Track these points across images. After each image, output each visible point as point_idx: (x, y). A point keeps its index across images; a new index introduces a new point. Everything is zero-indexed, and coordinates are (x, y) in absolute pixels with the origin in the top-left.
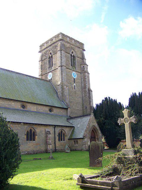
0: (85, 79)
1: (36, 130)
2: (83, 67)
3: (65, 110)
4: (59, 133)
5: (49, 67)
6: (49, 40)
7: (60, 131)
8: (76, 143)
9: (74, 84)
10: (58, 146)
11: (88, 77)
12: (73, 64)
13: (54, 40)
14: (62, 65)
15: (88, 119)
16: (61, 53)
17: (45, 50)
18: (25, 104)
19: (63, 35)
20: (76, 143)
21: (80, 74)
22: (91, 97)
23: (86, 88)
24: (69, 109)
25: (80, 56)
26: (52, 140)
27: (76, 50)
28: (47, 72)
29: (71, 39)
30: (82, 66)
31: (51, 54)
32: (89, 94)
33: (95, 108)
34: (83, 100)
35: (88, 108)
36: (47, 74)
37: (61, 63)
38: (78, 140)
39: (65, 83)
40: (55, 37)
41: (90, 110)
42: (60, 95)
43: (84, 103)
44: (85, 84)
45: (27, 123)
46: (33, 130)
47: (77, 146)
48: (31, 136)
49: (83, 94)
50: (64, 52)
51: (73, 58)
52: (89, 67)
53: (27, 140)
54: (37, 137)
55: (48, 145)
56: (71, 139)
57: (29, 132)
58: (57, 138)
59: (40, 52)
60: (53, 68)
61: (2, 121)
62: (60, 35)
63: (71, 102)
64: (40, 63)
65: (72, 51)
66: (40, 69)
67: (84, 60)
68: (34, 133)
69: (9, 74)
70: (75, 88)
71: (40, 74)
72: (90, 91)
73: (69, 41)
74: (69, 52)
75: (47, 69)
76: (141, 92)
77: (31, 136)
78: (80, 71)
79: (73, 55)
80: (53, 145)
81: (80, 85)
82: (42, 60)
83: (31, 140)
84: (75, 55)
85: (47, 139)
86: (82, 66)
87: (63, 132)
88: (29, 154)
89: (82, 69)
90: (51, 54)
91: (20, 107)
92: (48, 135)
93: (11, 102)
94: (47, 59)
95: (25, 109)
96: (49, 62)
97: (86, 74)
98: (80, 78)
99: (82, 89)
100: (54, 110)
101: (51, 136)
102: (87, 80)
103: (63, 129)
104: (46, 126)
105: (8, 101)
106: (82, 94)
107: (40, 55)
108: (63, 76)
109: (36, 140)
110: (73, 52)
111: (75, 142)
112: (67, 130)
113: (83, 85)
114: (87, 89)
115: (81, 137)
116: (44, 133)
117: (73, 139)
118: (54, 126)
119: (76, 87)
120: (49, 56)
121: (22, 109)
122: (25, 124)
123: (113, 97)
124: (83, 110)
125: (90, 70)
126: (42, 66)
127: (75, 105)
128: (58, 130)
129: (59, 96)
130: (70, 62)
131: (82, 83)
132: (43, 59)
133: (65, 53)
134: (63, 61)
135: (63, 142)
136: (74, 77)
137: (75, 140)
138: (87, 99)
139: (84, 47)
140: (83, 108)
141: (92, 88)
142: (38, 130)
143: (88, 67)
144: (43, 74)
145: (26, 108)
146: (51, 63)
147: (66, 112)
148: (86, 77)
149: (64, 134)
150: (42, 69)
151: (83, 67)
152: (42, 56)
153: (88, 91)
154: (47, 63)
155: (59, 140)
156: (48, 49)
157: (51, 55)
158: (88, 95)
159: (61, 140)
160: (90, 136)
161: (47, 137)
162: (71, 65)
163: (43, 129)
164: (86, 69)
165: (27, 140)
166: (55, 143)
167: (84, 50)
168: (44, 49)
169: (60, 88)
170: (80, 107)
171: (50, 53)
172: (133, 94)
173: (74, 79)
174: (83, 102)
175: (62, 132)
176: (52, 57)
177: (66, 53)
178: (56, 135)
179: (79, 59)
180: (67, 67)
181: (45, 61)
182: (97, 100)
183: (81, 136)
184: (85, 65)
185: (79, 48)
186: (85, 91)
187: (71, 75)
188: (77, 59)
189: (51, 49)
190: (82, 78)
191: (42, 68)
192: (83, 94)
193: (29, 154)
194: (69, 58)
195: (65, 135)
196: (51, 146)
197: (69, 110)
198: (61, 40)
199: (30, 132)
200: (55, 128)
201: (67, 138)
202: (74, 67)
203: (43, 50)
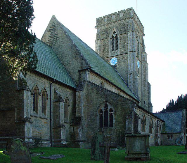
2: (144, 56)
8: (170, 138)
20: (170, 138)
25: (142, 43)
28: (109, 56)
34: (142, 94)
38: (174, 135)
47: (171, 141)
52: (148, 57)
69: (88, 48)
72: (149, 85)
76: (184, 95)
90: (114, 33)
107: (96, 30)
113: (143, 77)
114: (146, 83)
115: (178, 131)
138: (147, 94)
143: (147, 55)
151: (144, 56)
154: (109, 44)
157: (114, 35)
158: (147, 89)
171: (113, 32)
186: (145, 85)
190: (143, 69)
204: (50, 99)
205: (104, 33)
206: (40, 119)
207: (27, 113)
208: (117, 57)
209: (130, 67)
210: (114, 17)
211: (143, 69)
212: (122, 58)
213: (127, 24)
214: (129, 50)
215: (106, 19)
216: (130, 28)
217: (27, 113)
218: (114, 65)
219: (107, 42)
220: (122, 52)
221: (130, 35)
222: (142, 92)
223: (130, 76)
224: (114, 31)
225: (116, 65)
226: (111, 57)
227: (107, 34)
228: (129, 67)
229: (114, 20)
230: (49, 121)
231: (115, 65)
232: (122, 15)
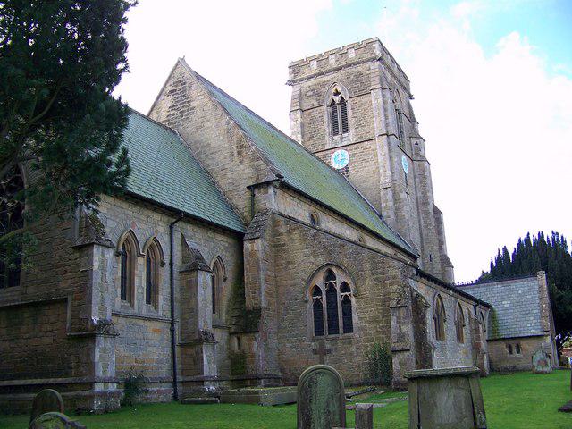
2: (416, 143)
6: (329, 53)
8: (514, 350)
13: (352, 55)
16: (384, 96)
17: (315, 81)
20: (514, 350)
30: (414, 141)
31: (337, 93)
38: (524, 344)
40: (357, 47)
47: (519, 359)
56: (496, 340)
59: (291, 83)
75: (327, 138)
111: (510, 348)
113: (419, 194)
115: (533, 332)
117: (504, 339)
126: (302, 125)
129: (389, 222)
137: (510, 342)
141: (440, 199)
151: (416, 143)
152: (301, 97)
153: (432, 213)
154: (326, 118)
156: (326, 78)
157: (337, 99)
158: (433, 224)
167: (411, 97)
171: (334, 91)
181: (316, 113)
186: (426, 213)
204: (171, 264)
206: (141, 322)
207: (102, 309)
208: (348, 148)
210: (332, 59)
217: (102, 309)
219: (320, 115)
228: (381, 171)
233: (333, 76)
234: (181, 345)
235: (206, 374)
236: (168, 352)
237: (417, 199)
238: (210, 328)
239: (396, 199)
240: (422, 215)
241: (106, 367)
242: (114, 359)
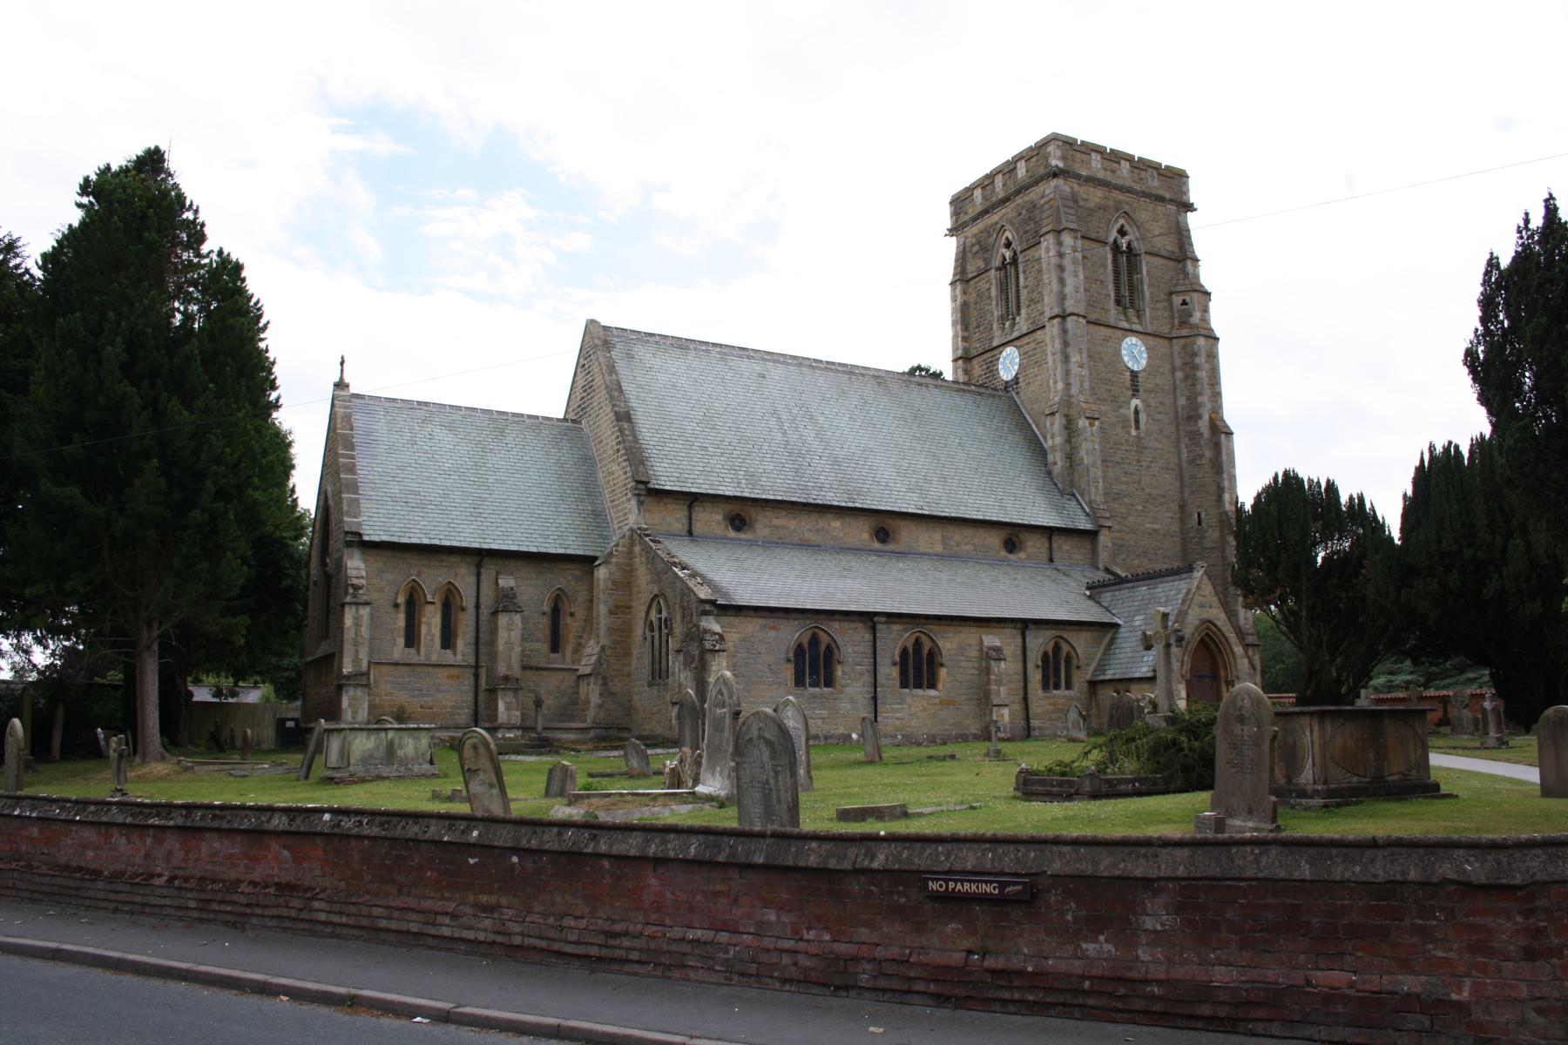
0: (1195, 367)
1: (940, 643)
2: (1184, 303)
3: (1086, 546)
4: (1045, 654)
5: (1003, 319)
7: (1051, 645)
9: (1135, 402)
10: (1039, 710)
11: (1213, 356)
12: (1128, 296)
14: (1069, 311)
15: (1179, 590)
16: (1060, 243)
18: (888, 521)
19: (1068, 144)
21: (1165, 343)
22: (1225, 466)
23: (1200, 417)
24: (1104, 532)
26: (1013, 686)
27: (1143, 216)
28: (995, 344)
29: (1115, 157)
30: (1177, 300)
31: (1008, 245)
32: (1217, 447)
33: (1466, 454)
34: (1182, 482)
35: (1210, 518)
36: (996, 352)
37: (1062, 297)
39: (1080, 399)
41: (1221, 531)
42: (1059, 464)
43: (1186, 495)
44: (1196, 397)
45: (900, 616)
46: (824, 639)
48: (918, 668)
49: (1184, 450)
50: (1076, 238)
51: (1127, 260)
52: (1213, 306)
53: (904, 685)
54: (943, 672)
55: (995, 709)
57: (1051, 655)
58: (1035, 676)
60: (1023, 325)
61: (173, 239)
62: (1051, 148)
63: (1118, 497)
64: (958, 291)
65: (1122, 221)
66: (959, 327)
67: (1189, 263)
68: (931, 653)
70: (1137, 422)
71: (960, 353)
72: (1220, 432)
73: (1100, 175)
74: (1102, 236)
75: (995, 326)
77: (918, 668)
78: (1165, 330)
79: (1124, 242)
80: (1018, 707)
81: (1168, 400)
82: (962, 278)
83: (918, 686)
84: (1135, 244)
85: (988, 683)
86: (1177, 300)
87: (1065, 648)
88: (911, 741)
89: (1176, 314)
91: (866, 536)
92: (992, 662)
93: (829, 516)
94: (993, 273)
95: (891, 547)
96: (1003, 288)
97: (1201, 341)
98: (1168, 367)
99: (1178, 426)
100: (1029, 543)
101: (1007, 668)
102: (1203, 374)
103: (1065, 635)
104: (984, 624)
105: (814, 516)
106: (1179, 453)
107: (952, 245)
108: (1074, 369)
109: (940, 686)
110: (1127, 228)
112: (1081, 643)
113: (1182, 401)
114: (1203, 426)
116: (974, 653)
117: (1111, 681)
118: (1019, 626)
119: (1143, 417)
120: (999, 258)
121: (877, 545)
122: (891, 620)
123: (1312, 471)
124: (1184, 534)
125: (1220, 318)
127: (1140, 508)
128: (1039, 643)
130: (1111, 287)
131: (1175, 389)
132: (972, 269)
133: (1079, 243)
134: (1068, 290)
135: (1067, 693)
136: (1130, 365)
137: (432, 579)
139: (1186, 193)
140: (1182, 521)
142: (948, 643)
144: (974, 353)
145: (894, 539)
146: (1012, 296)
147: (1089, 547)
148: (1201, 360)
149: (1068, 659)
150: (965, 327)
151: (1184, 303)
154: (994, 292)
155: (1045, 687)
157: (1008, 254)
158: (1208, 454)
159: (1057, 687)
160: (1187, 667)
161: (988, 674)
162: (1118, 302)
163: (969, 636)
164: (1197, 315)
165: (904, 685)
166: (1025, 699)
167: (1189, 207)
168: (975, 219)
169: (1056, 428)
170: (1165, 520)
171: (1003, 241)
172: (1432, 448)
173: (1134, 375)
174: (1182, 492)
175: (1057, 648)
176: (1014, 260)
177: (1087, 243)
178: (1030, 665)
179: (1162, 261)
180: (1093, 317)
181: (983, 285)
182: (1248, 487)
183: (1145, 669)
184: (1195, 295)
185: (1161, 199)
186: (1195, 436)
187: (1118, 354)
188: (1146, 265)
189: (1012, 224)
191: (966, 318)
192: (1184, 450)
193: (911, 741)
194: (1104, 266)
195: (1075, 662)
196: (1006, 711)
197: (1104, 539)
198: (1055, 175)
199: (914, 650)
200: (1028, 633)
201: (1080, 679)
202: (1131, 312)
203: (965, 225)
204: (477, 607)
205: (976, 253)
206: (430, 669)
207: (356, 661)
208: (1018, 343)
209: (1055, 383)
210: (1022, 170)
211: (1178, 362)
212: (1033, 345)
213: (1042, 202)
214: (1048, 314)
215: (978, 193)
216: (1050, 220)
217: (356, 661)
218: (1124, 345)
219: (987, 286)
220: (1034, 322)
221: (1048, 250)
222: (1181, 471)
223: (1052, 424)
224: (1007, 238)
225: (1016, 379)
226: (1001, 349)
227: (986, 255)
228: (1051, 383)
229: (1001, 195)
230: (469, 674)
231: (1012, 380)
232: (1024, 170)
233: (1000, 214)
234: (486, 690)
235: (500, 721)
236: (471, 697)
237: (1176, 412)
238: (516, 671)
239: (1069, 427)
240: (1185, 441)
241: (355, 713)
242: (366, 705)
